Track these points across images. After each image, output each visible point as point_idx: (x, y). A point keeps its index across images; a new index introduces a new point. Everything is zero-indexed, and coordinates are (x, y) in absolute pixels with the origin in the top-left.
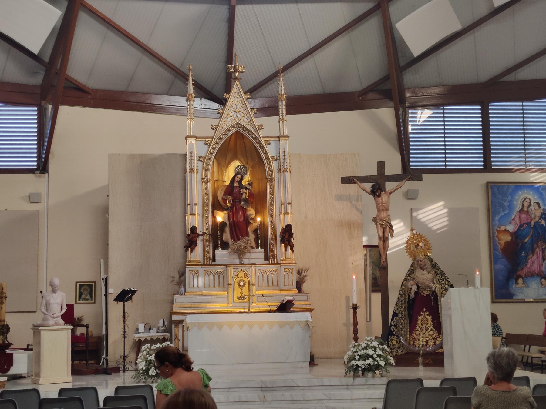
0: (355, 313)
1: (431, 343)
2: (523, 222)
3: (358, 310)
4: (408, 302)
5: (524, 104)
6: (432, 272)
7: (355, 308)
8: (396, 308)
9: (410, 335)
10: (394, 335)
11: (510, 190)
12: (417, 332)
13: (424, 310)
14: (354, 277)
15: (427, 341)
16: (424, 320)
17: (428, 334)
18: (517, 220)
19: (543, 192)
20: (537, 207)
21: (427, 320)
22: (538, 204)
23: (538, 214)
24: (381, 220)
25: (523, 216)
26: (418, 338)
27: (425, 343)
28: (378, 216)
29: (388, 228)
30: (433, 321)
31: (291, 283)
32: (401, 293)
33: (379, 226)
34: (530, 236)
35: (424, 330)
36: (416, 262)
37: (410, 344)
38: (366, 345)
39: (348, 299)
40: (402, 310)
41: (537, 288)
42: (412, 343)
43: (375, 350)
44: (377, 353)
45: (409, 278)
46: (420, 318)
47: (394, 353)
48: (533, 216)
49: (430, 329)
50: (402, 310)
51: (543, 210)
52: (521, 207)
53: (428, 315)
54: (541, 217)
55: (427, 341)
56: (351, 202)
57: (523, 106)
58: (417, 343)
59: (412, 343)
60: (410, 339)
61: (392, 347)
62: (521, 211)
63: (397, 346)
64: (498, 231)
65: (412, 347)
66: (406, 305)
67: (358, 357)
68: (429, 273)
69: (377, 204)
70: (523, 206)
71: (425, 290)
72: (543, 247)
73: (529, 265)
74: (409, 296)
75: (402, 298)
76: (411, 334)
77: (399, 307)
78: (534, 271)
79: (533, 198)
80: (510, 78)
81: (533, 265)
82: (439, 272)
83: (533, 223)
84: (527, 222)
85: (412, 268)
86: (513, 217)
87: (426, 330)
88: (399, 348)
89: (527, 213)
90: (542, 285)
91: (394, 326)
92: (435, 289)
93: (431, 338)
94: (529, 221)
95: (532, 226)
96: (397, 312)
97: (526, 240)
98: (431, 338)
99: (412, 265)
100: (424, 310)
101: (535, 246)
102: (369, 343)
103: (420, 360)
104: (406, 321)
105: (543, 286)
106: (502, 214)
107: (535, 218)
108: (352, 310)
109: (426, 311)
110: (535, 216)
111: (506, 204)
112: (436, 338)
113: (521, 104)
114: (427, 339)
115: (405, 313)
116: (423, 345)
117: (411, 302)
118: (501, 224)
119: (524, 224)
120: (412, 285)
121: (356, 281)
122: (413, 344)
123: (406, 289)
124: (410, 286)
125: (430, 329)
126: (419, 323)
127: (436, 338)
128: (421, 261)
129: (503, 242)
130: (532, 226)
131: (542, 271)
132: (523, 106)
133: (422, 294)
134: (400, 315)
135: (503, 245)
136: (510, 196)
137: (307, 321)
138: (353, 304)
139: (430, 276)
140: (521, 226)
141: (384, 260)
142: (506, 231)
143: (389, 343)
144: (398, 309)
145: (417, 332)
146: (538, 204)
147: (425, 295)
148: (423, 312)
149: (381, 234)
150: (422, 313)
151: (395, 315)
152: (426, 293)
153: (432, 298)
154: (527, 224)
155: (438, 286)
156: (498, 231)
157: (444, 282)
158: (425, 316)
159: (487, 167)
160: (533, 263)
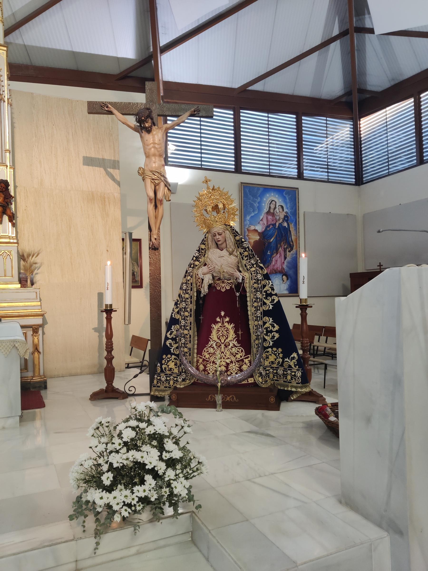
0: (109, 319)
1: (234, 367)
2: (269, 223)
3: (113, 314)
4: (197, 301)
5: (269, 115)
6: (235, 253)
7: (109, 311)
8: (176, 310)
9: (197, 354)
10: (172, 354)
11: (260, 192)
12: (211, 350)
13: (223, 313)
14: (109, 263)
15: (228, 364)
16: (223, 331)
17: (228, 353)
18: (265, 221)
19: (286, 196)
20: (281, 210)
21: (227, 330)
22: (282, 207)
23: (282, 216)
24: (151, 171)
25: (270, 217)
26: (212, 359)
27: (224, 368)
28: (146, 165)
29: (162, 185)
30: (235, 332)
31: (9, 273)
32: (185, 287)
33: (148, 181)
34: (274, 237)
35: (223, 346)
36: (210, 236)
37: (198, 369)
38: (133, 434)
39: (101, 296)
40: (186, 314)
41: (279, 284)
42: (201, 367)
43: (161, 448)
44: (166, 456)
45: (197, 263)
46: (215, 327)
47: (171, 383)
48: (278, 218)
49: (231, 345)
50: (186, 314)
51: (286, 213)
52: (268, 209)
53: (228, 322)
54: (284, 220)
55: (228, 364)
56: (105, 170)
57: (268, 117)
58: (210, 368)
59: (201, 367)
60: (198, 361)
61: (168, 372)
62: (268, 213)
63: (176, 371)
64: (248, 230)
65: (202, 375)
66: (193, 307)
67: (110, 475)
68: (231, 254)
69: (145, 144)
70: (270, 207)
71: (223, 282)
72: (285, 247)
73: (273, 264)
74: (199, 292)
75: (187, 296)
76: (200, 352)
77: (181, 309)
78: (277, 269)
79: (279, 201)
80: (258, 87)
81: (276, 263)
82: (246, 253)
83: (277, 225)
84: (272, 223)
85: (203, 247)
86: (261, 217)
87: (226, 346)
88: (180, 374)
89: (273, 215)
90: (283, 281)
91: (172, 339)
92: (243, 279)
93: (233, 359)
94: (275, 222)
95: (277, 227)
96: (178, 317)
97: (271, 240)
98: (233, 359)
99: (203, 243)
100: (223, 313)
101: (279, 245)
102: (143, 425)
103: (219, 398)
104: (192, 332)
105: (284, 282)
106: (253, 214)
107: (279, 220)
108: (105, 315)
109: (225, 316)
110: (280, 218)
111: (256, 205)
112: (242, 360)
113: (266, 115)
114: (228, 361)
115: (191, 319)
116: (221, 372)
117: (201, 302)
118: (251, 224)
119: (270, 224)
120: (204, 274)
121: (111, 272)
122: (205, 370)
123: (193, 280)
124: (201, 276)
125: (231, 345)
126: (214, 335)
127: (242, 360)
128: (220, 234)
129: (252, 241)
130: (277, 227)
131: (284, 269)
132: (268, 117)
133: (218, 288)
134: (183, 323)
135: (252, 244)
136: (259, 198)
137: (15, 341)
138: (106, 305)
139: (233, 260)
140: (268, 226)
141: (155, 237)
142: (256, 231)
143: (164, 366)
144: (178, 312)
145: (211, 350)
146: (282, 207)
147: (223, 290)
148: (221, 317)
149: (152, 194)
150: (218, 319)
151: (173, 321)
152: (224, 287)
153: (238, 294)
154: (273, 225)
155: (247, 275)
156: (248, 230)
157: (253, 269)
158: (223, 323)
159: (238, 169)
160: (276, 261)
